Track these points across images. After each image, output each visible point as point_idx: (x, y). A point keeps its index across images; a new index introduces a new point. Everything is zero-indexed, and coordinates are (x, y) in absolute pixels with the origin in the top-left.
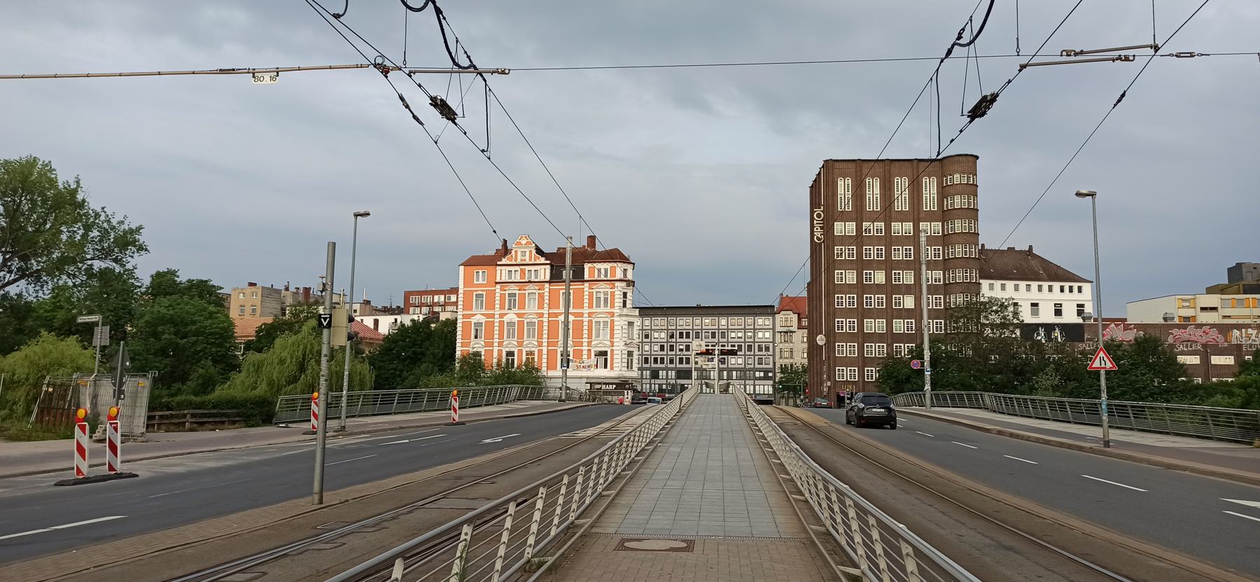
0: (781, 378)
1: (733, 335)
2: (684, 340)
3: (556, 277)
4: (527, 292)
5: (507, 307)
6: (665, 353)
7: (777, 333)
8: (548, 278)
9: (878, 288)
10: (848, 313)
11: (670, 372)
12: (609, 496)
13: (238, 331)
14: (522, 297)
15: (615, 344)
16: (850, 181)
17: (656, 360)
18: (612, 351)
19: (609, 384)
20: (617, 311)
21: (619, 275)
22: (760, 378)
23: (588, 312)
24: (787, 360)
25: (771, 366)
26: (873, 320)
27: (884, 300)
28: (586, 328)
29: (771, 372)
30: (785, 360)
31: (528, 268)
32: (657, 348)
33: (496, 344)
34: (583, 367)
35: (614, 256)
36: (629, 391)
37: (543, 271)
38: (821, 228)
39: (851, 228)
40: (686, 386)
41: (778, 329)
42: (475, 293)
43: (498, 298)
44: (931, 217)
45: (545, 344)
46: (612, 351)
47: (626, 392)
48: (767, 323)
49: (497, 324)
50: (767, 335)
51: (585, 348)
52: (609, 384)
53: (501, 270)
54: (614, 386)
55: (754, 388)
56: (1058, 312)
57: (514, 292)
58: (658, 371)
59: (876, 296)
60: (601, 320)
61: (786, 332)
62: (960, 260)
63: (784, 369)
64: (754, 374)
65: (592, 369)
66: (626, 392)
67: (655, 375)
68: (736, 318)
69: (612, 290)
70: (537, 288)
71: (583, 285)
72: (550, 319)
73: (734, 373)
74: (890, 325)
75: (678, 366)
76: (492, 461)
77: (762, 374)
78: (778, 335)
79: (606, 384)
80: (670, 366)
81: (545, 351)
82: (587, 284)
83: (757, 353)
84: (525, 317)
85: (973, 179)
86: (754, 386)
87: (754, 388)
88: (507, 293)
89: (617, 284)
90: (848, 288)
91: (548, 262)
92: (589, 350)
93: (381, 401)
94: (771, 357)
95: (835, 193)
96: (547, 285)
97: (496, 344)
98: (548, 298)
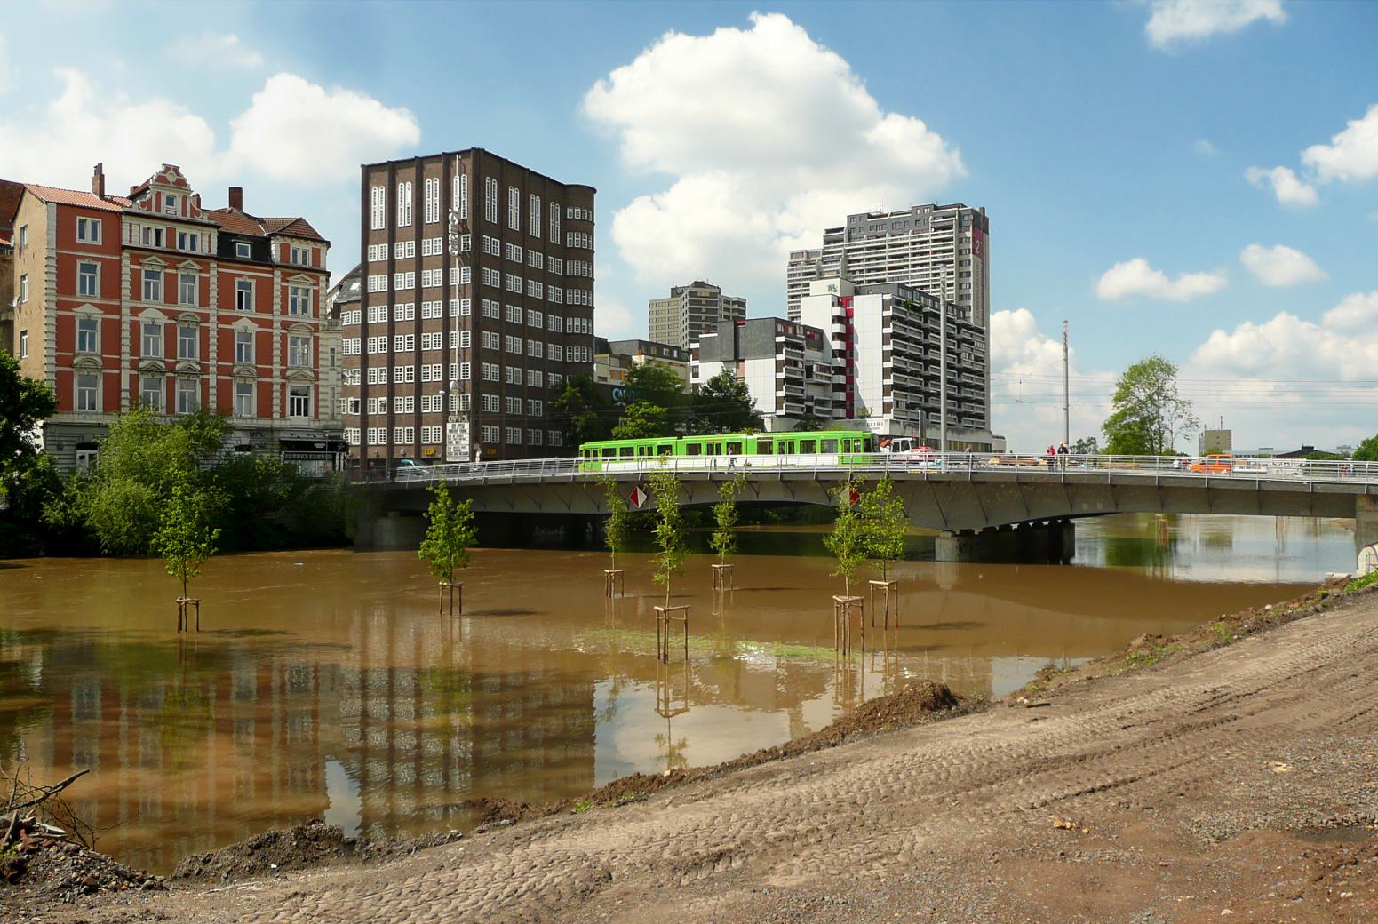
8: (214, 251)
12: (30, 816)
15: (321, 376)
18: (317, 387)
28: (277, 345)
31: (180, 229)
37: (206, 238)
42: (79, 263)
46: (317, 387)
56: (951, 273)
69: (316, 288)
70: (198, 267)
81: (213, 383)
82: (277, 272)
85: (588, 214)
92: (283, 385)
94: (375, 443)
96: (213, 265)
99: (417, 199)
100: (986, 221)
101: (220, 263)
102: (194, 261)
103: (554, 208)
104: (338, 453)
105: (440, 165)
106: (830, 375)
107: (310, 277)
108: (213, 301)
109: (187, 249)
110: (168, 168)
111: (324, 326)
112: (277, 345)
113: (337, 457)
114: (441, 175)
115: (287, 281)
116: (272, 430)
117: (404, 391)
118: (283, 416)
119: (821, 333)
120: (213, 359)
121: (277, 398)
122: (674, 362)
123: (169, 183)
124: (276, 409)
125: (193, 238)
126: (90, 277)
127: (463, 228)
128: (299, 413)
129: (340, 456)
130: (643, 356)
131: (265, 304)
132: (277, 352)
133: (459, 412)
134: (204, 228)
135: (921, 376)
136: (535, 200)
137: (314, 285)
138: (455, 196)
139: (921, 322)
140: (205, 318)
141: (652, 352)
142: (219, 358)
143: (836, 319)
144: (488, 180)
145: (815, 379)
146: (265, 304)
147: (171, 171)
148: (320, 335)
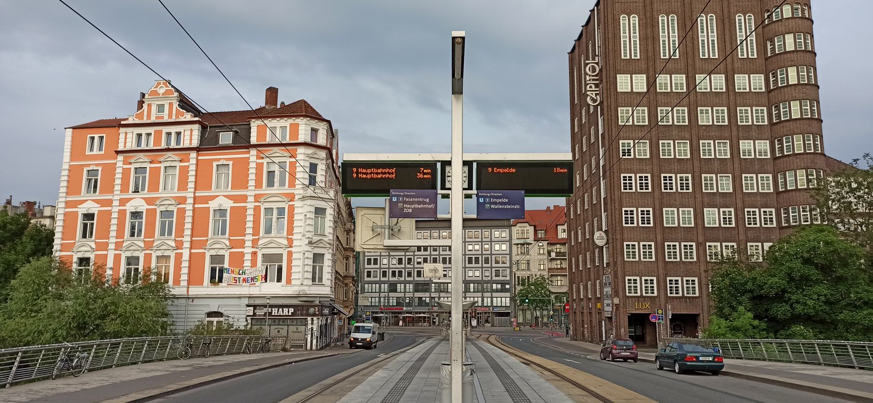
0: (521, 290)
1: (470, 247)
2: (422, 253)
3: (208, 144)
4: (162, 166)
5: (132, 188)
6: (403, 266)
7: (513, 246)
9: (679, 165)
10: (639, 199)
11: (408, 285)
14: (155, 172)
15: (295, 243)
16: (637, 19)
17: (394, 274)
19: (283, 306)
20: (298, 191)
21: (304, 135)
22: (497, 291)
23: (253, 193)
24: (524, 272)
25: (508, 278)
26: (675, 209)
27: (690, 182)
28: (250, 218)
29: (508, 284)
30: (522, 273)
31: (165, 129)
32: (395, 261)
33: (112, 246)
34: (244, 280)
35: (302, 110)
36: (315, 318)
37: (188, 133)
38: (597, 86)
39: (640, 83)
40: (424, 299)
41: (515, 241)
43: (119, 176)
44: (749, 67)
45: (187, 245)
46: (290, 254)
47: (309, 319)
48: (504, 235)
49: (115, 215)
50: (504, 247)
51: (248, 250)
52: (283, 306)
53: (126, 133)
54: (292, 310)
55: (492, 301)
57: (143, 165)
58: (396, 284)
59: (679, 175)
60: (274, 206)
61: (523, 244)
62: (798, 122)
63: (522, 282)
64: (492, 287)
65: (258, 283)
66: (309, 319)
67: (393, 288)
68: (473, 231)
70: (177, 158)
71: (249, 152)
72: (196, 206)
73: (472, 285)
74: (699, 216)
75: (417, 279)
77: (499, 286)
78: (514, 248)
79: (279, 306)
80: (383, 279)
81: (186, 256)
82: (253, 152)
83: (494, 265)
84: (158, 203)
86: (492, 298)
87: (492, 301)
88: (132, 167)
89: (301, 150)
90: (639, 165)
91: (197, 119)
95: (617, 37)
96: (193, 155)
97: (112, 246)
98: (194, 173)
125: (178, 134)
126: (143, 177)
131: (240, 181)
132: (250, 225)
144: (739, 18)
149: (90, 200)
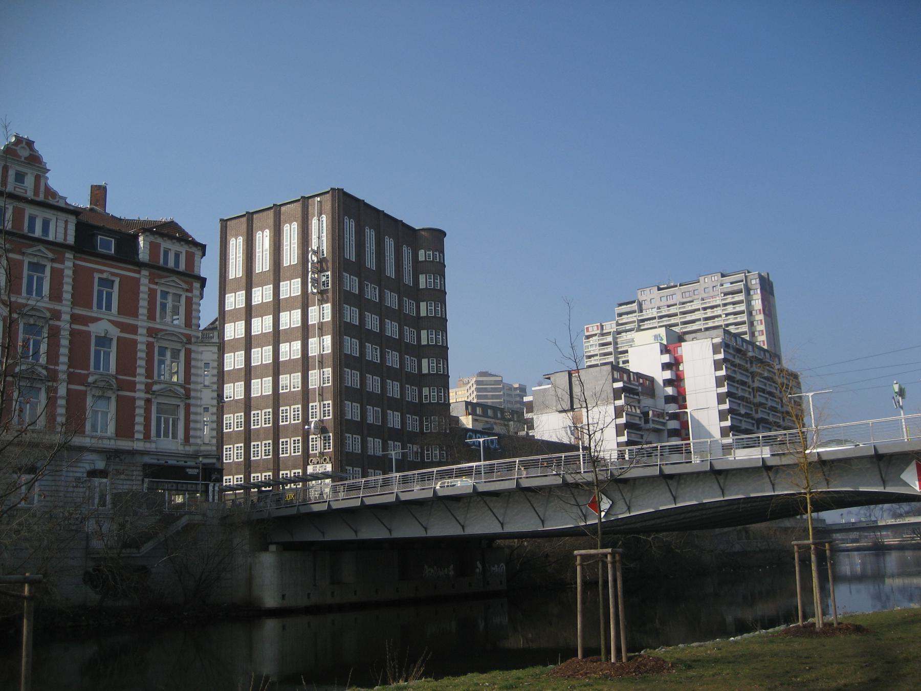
4: (26, 261)
8: (71, 240)
13: (915, 471)
28: (142, 355)
31: (29, 210)
37: (61, 224)
58: (614, 389)
69: (189, 295)
70: (50, 255)
76: (563, 525)
81: (62, 391)
82: (145, 272)
93: (455, 474)
96: (69, 255)
99: (274, 250)
100: (771, 285)
101: (76, 255)
102: (47, 248)
103: (406, 251)
104: (211, 484)
105: (297, 207)
106: (664, 421)
107: (182, 281)
108: (67, 296)
109: (38, 233)
110: (19, 140)
111: (198, 338)
112: (142, 355)
113: (211, 488)
114: (300, 219)
115: (156, 283)
116: (133, 453)
117: (234, 471)
118: (147, 437)
119: (652, 380)
120: (63, 363)
121: (140, 415)
122: (498, 421)
123: (20, 157)
124: (139, 428)
127: (321, 266)
128: (166, 435)
129: (214, 487)
130: (470, 416)
131: (129, 306)
132: (141, 363)
133: (320, 453)
134: (59, 214)
135: (753, 418)
136: (389, 243)
137: (187, 291)
138: (313, 237)
139: (748, 365)
140: (56, 315)
141: (478, 412)
142: (75, 303)
143: (665, 367)
145: (651, 425)
146: (129, 306)
147: (24, 144)
148: (193, 347)
149: (107, 320)
